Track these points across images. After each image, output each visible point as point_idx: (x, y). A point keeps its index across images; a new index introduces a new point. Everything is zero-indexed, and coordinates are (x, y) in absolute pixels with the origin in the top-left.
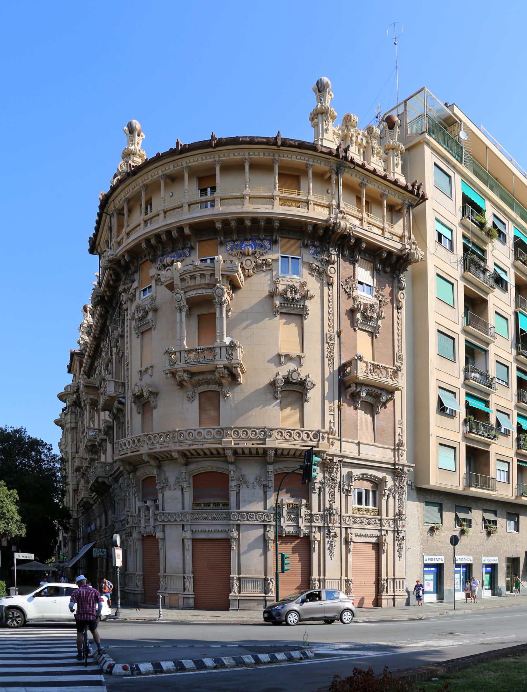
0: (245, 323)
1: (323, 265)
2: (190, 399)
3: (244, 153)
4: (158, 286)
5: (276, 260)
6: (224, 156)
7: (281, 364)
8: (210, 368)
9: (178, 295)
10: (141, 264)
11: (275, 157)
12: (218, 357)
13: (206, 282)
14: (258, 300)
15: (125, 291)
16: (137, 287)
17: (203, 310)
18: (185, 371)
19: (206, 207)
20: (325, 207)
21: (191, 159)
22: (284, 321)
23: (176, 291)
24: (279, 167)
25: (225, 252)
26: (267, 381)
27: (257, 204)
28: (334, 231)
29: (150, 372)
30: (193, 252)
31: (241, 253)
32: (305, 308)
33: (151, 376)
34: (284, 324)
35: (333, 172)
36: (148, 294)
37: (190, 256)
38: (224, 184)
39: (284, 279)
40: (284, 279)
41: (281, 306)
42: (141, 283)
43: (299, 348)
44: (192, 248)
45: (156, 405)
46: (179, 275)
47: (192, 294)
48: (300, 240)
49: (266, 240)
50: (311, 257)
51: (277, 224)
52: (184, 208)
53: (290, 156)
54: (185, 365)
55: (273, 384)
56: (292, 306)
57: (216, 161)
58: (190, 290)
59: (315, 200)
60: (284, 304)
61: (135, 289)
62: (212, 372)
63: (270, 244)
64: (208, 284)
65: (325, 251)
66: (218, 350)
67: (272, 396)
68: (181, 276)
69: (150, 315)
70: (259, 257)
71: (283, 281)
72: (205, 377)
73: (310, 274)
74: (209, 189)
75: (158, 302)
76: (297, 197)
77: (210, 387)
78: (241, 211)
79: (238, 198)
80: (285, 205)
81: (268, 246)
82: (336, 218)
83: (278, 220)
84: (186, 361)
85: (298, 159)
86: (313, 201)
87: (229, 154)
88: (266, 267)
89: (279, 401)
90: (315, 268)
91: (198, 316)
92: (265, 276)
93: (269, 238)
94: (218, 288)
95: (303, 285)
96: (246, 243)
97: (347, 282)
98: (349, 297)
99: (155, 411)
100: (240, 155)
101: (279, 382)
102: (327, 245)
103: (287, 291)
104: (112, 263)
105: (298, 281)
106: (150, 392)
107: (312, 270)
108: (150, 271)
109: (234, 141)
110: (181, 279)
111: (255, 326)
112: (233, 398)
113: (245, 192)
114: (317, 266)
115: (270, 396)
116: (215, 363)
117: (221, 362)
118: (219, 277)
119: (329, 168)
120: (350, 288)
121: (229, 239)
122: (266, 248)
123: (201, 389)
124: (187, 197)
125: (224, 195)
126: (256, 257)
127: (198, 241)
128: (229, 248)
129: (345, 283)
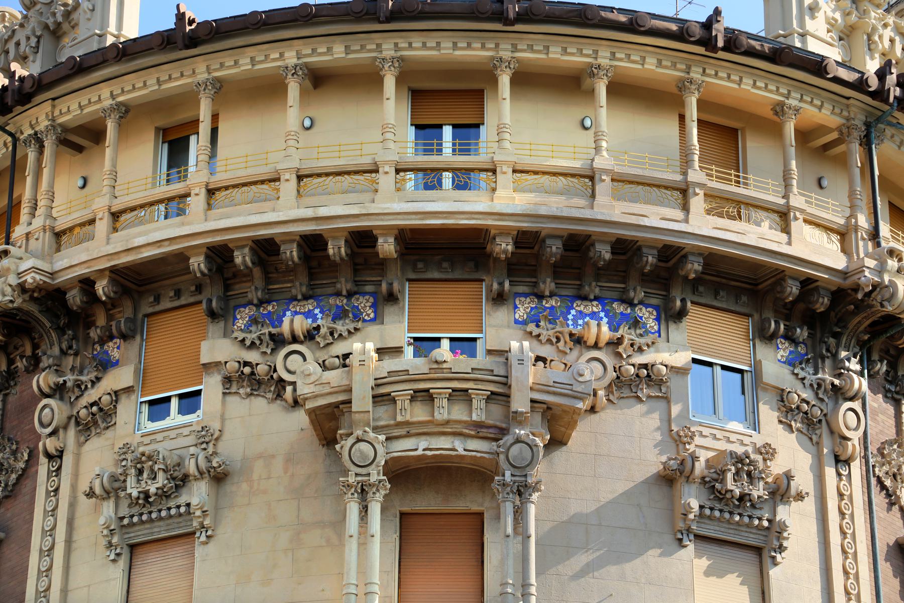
0: (581, 560)
1: (822, 400)
3: (596, 52)
4: (230, 399)
5: (681, 371)
6: (531, 48)
9: (363, 446)
10: (148, 316)
13: (475, 417)
14: (621, 487)
15: (59, 391)
16: (129, 390)
19: (439, 185)
20: (832, 230)
22: (703, 563)
23: (359, 432)
24: (698, 101)
28: (862, 306)
30: (390, 312)
32: (776, 532)
34: (708, 573)
35: (856, 134)
36: (175, 418)
37: (377, 319)
39: (706, 431)
40: (706, 431)
41: (701, 515)
42: (144, 377)
44: (392, 298)
46: (372, 383)
47: (405, 447)
48: (748, 315)
49: (647, 306)
50: (785, 370)
51: (694, 267)
53: (735, 77)
56: (737, 518)
57: (501, 60)
58: (408, 435)
59: (809, 210)
60: (712, 509)
61: (116, 395)
63: (658, 319)
64: (479, 425)
65: (823, 358)
68: (377, 385)
69: (198, 494)
70: (629, 356)
71: (701, 435)
73: (780, 422)
74: (447, 131)
75: (231, 449)
76: (733, 188)
78: (587, 214)
80: (720, 215)
81: (652, 324)
82: (881, 270)
83: (700, 254)
85: (759, 88)
86: (802, 211)
88: (648, 385)
90: (798, 408)
91: (402, 514)
92: (643, 415)
93: (654, 301)
94: (518, 441)
95: (768, 452)
97: (883, 455)
98: (891, 504)
102: (832, 341)
103: (724, 472)
104: (27, 296)
105: (747, 440)
107: (788, 410)
108: (205, 346)
110: (374, 397)
111: (613, 569)
113: (598, 163)
114: (804, 401)
118: (520, 404)
119: (844, 121)
120: (894, 476)
121: (521, 289)
122: (647, 332)
124: (391, 145)
125: (527, 161)
126: (619, 355)
128: (521, 313)
129: (879, 459)
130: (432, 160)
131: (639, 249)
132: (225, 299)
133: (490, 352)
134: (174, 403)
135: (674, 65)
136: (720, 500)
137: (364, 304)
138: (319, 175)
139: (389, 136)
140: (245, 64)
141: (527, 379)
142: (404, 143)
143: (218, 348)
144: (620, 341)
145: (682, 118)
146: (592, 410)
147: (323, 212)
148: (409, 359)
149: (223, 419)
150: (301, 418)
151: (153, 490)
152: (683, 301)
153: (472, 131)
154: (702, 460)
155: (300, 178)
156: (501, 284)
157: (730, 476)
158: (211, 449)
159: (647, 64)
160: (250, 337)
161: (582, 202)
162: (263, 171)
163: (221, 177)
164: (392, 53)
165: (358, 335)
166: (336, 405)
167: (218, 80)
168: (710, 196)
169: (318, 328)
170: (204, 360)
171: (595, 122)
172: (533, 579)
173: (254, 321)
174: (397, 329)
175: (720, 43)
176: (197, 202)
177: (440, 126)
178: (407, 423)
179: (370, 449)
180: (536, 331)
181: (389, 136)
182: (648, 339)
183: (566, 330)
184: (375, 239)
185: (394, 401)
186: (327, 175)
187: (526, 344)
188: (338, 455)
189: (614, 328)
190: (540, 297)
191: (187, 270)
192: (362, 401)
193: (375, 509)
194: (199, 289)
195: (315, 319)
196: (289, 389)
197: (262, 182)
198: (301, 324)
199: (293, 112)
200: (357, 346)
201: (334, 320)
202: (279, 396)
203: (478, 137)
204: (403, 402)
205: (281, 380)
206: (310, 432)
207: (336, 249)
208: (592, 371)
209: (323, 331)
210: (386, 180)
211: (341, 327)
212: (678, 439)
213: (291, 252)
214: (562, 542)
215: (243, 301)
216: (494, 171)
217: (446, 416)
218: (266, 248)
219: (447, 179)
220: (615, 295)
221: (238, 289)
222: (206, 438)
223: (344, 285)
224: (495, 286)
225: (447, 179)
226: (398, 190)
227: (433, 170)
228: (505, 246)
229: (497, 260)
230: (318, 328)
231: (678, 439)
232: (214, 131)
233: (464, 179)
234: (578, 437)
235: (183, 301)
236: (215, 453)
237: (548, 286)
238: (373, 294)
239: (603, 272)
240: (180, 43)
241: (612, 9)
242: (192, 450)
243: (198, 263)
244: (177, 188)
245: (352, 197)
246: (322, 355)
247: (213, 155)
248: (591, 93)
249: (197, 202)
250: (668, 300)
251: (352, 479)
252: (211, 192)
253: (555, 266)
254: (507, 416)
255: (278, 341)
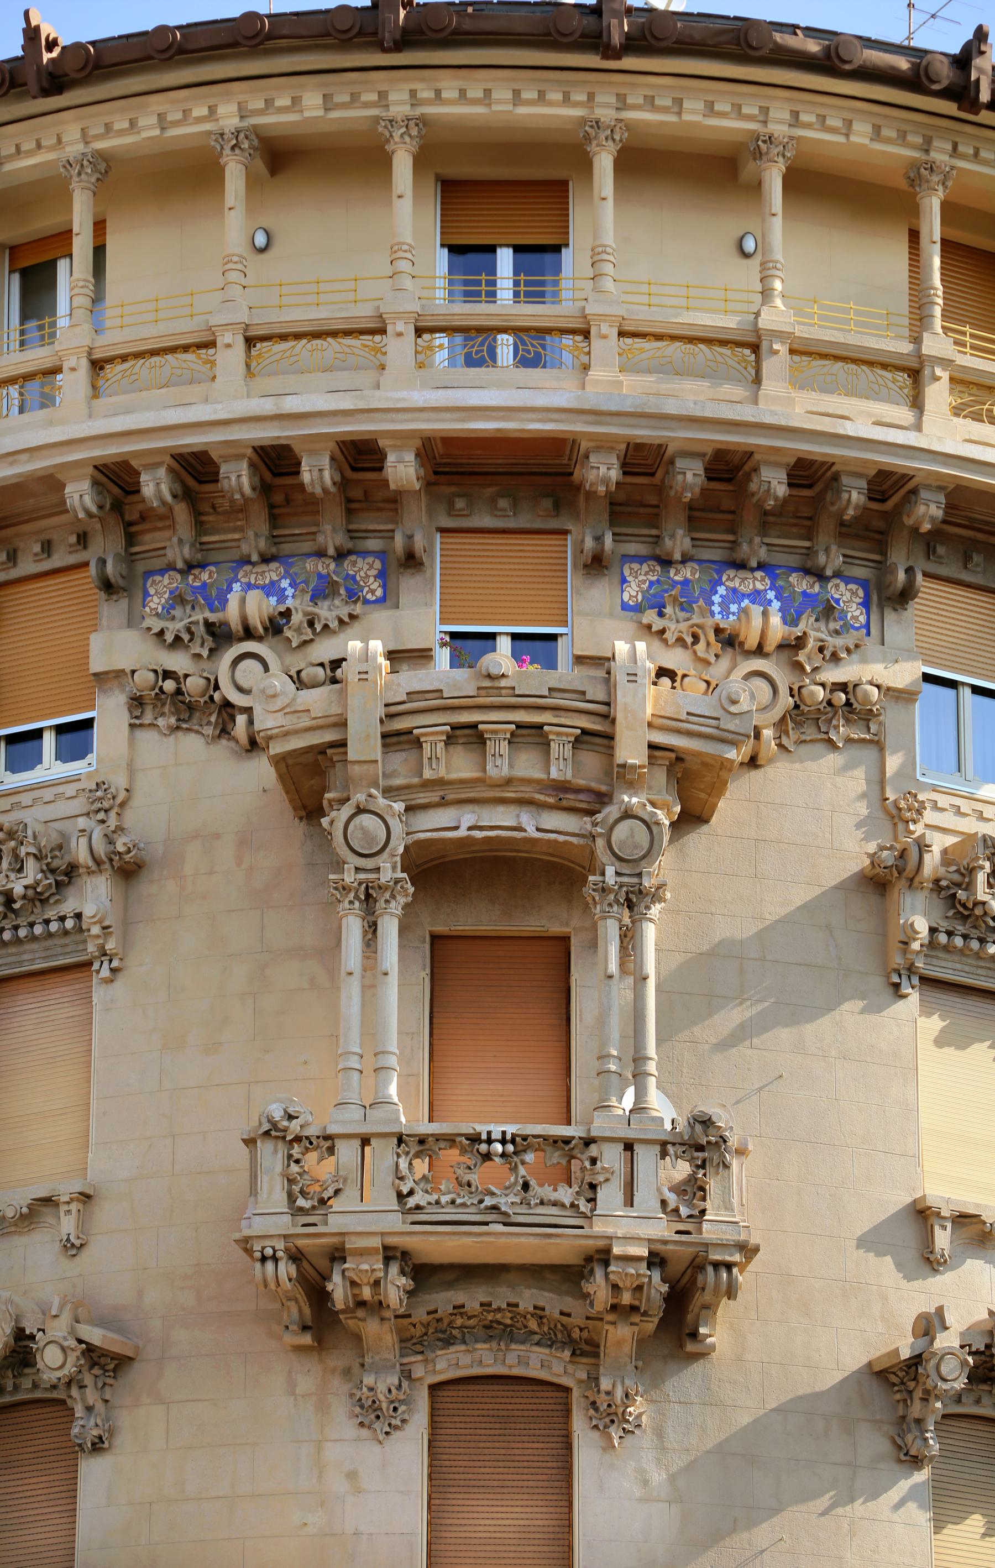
0: (733, 1016)
2: (376, 1416)
3: (765, 110)
4: (145, 736)
5: (904, 696)
7: (931, 1262)
8: (562, 1248)
9: (367, 821)
11: (935, 155)
12: (611, 1196)
14: (801, 895)
17: (504, 924)
18: (390, 1254)
19: (491, 357)
21: (450, 85)
22: (935, 1024)
23: (359, 797)
24: (945, 205)
25: (611, 615)
26: (854, 1357)
27: (827, 389)
29: (68, 1225)
30: (408, 584)
31: (718, 631)
33: (73, 1248)
34: (940, 1042)
36: (50, 767)
37: (387, 599)
38: (626, 256)
39: (943, 801)
40: (943, 801)
41: (932, 944)
43: (590, 698)
44: (411, 561)
45: (111, 1432)
46: (381, 711)
49: (848, 580)
51: (929, 511)
52: (390, 342)
54: (395, 1222)
55: (899, 1379)
58: (443, 803)
60: (950, 934)
62: (571, 1275)
63: (866, 604)
64: (561, 787)
66: (612, 1157)
67: (884, 1446)
68: (390, 716)
69: (94, 898)
70: (815, 669)
71: (936, 807)
72: (501, 1295)
74: (505, 258)
75: (146, 823)
77: (511, 1358)
78: (747, 413)
79: (723, 343)
81: (855, 612)
83: (941, 488)
84: (401, 1197)
87: (679, 102)
88: (848, 721)
89: (922, 1476)
91: (435, 938)
93: (861, 572)
94: (628, 815)
96: (732, 579)
99: (93, 1473)
100: (742, 117)
101: (950, 1367)
103: (971, 871)
106: (92, 1355)
108: (96, 642)
109: (739, 43)
110: (384, 736)
111: (784, 1034)
112: (659, 1433)
113: (768, 320)
115: (874, 1442)
116: (599, 1227)
117: (632, 1225)
118: (630, 750)
121: (633, 548)
122: (847, 627)
123: (451, 1363)
124: (408, 283)
126: (799, 667)
127: (443, 531)
128: (632, 592)
130: (478, 312)
131: (836, 478)
132: (130, 558)
133: (580, 660)
134: (49, 740)
135: (903, 135)
136: (965, 918)
137: (364, 570)
138: (283, 337)
139: (403, 265)
140: (148, 127)
141: (643, 709)
142: (429, 278)
143: (121, 646)
144: (800, 643)
145: (914, 236)
146: (753, 762)
147: (292, 404)
148: (442, 670)
149: (131, 771)
150: (261, 771)
151: (18, 890)
152: (909, 571)
153: (548, 257)
154: (936, 850)
155: (250, 342)
156: (599, 539)
157: (981, 878)
158: (112, 822)
159: (855, 133)
160: (173, 628)
161: (737, 391)
162: (184, 328)
163: (113, 339)
164: (406, 110)
165: (356, 627)
166: (321, 750)
167: (102, 156)
168: (960, 381)
169: (287, 614)
170: (96, 665)
171: (763, 244)
172: (651, 1049)
173: (178, 599)
174: (422, 617)
175: (985, 96)
176: (73, 382)
177: (492, 249)
178: (440, 783)
179: (379, 826)
180: (658, 624)
181: (403, 265)
182: (848, 640)
183: (709, 623)
184: (380, 456)
185: (418, 744)
186: (298, 336)
187: (641, 646)
188: (325, 837)
189: (790, 619)
190: (666, 562)
191: (61, 508)
192: (364, 743)
193: (390, 928)
194: (83, 540)
195: (282, 598)
196: (241, 719)
197: (186, 348)
198: (258, 607)
199: (236, 214)
200: (355, 646)
201: (314, 599)
202: (225, 731)
203: (557, 270)
204: (433, 745)
205: (227, 704)
206: (279, 800)
207: (317, 473)
208: (751, 693)
209: (297, 618)
210: (400, 347)
211: (327, 612)
212: (897, 815)
213: (238, 478)
214: (704, 983)
215: (158, 563)
216: (586, 334)
217: (505, 772)
218: (195, 470)
219: (505, 345)
220: (793, 560)
221: (149, 541)
222: (105, 802)
223: (331, 537)
224: (589, 543)
225: (505, 345)
226: (421, 366)
227: (480, 330)
228: (603, 472)
229: (591, 495)
230: (287, 614)
231: (897, 815)
232: (99, 252)
233: (534, 345)
234: (727, 810)
235: (57, 561)
236: (120, 829)
237: (678, 541)
238: (382, 555)
239: (770, 520)
240: (33, 86)
241: (793, 29)
242: (82, 822)
243: (80, 495)
244: (37, 357)
245: (342, 379)
246: (296, 662)
247: (98, 297)
248: (756, 188)
249: (73, 382)
250: (883, 568)
251: (349, 877)
252: (97, 365)
253: (691, 507)
254: (608, 773)
255: (220, 635)
